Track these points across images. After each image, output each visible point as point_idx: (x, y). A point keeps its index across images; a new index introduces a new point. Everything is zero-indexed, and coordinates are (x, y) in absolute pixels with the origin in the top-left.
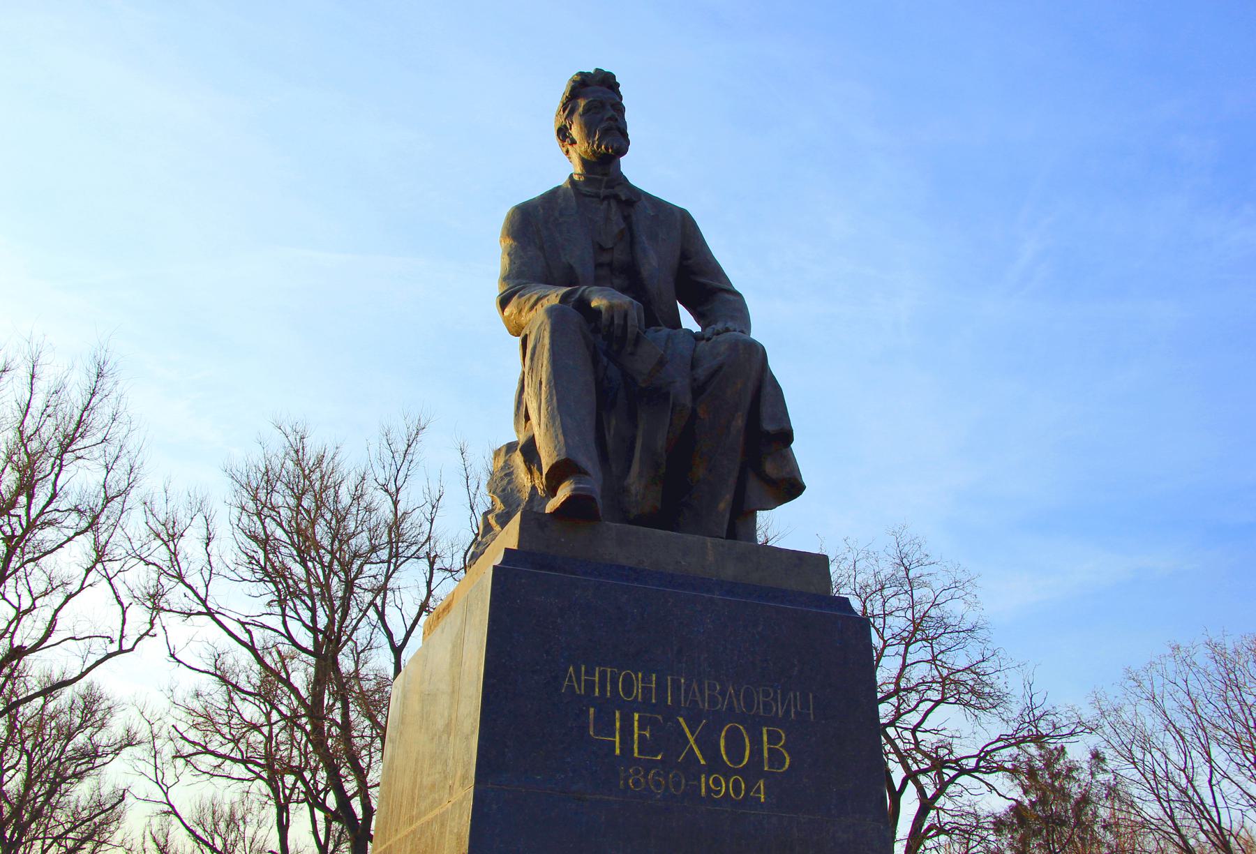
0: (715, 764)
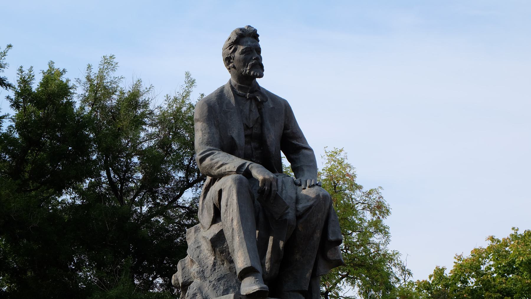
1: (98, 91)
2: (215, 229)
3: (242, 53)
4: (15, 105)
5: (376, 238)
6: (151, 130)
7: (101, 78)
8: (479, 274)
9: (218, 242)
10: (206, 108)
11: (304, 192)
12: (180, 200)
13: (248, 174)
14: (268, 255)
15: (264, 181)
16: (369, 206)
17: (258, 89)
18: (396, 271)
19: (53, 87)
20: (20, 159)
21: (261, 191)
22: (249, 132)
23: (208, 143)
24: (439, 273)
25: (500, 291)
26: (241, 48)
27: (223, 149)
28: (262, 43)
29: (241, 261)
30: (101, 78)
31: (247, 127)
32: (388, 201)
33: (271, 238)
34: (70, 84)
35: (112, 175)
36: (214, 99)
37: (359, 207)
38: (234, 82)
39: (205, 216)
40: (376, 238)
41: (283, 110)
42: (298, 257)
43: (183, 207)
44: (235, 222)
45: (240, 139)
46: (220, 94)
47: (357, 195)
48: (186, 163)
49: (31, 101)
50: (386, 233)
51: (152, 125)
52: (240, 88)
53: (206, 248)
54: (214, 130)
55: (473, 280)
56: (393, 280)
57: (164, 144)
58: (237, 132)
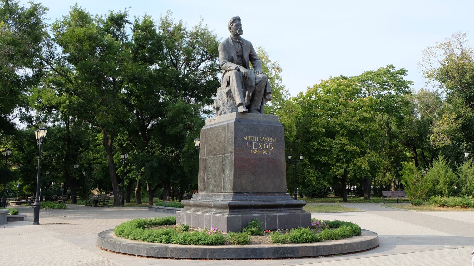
0: (263, 149)
1: (165, 25)
2: (228, 89)
3: (235, 26)
4: (134, 31)
5: (277, 81)
6: (187, 39)
7: (166, 19)
8: (316, 94)
9: (229, 93)
10: (223, 46)
11: (258, 76)
12: (199, 68)
13: (239, 70)
14: (246, 98)
15: (245, 73)
16: (274, 68)
17: (240, 39)
18: (284, 93)
19: (148, 23)
20: (136, 52)
21: (244, 76)
22: (238, 54)
23: (224, 59)
24: (301, 94)
25: (324, 101)
26: (235, 24)
27: (229, 61)
28: (242, 22)
29: (238, 101)
30: (166, 19)
31: (237, 53)
32: (281, 67)
33: (247, 92)
34: (154, 21)
35: (172, 58)
36: (225, 43)
37: (270, 69)
38: (232, 36)
39: (224, 84)
40: (277, 81)
41: (250, 46)
42: (256, 98)
43: (201, 70)
44: (235, 87)
45: (235, 58)
46: (228, 41)
47: (269, 64)
48: (201, 52)
49: (139, 29)
50: (281, 79)
51: (187, 37)
52: (234, 38)
53: (224, 96)
54: (226, 54)
55: (314, 96)
56: (283, 97)
57: (192, 45)
58: (234, 55)
